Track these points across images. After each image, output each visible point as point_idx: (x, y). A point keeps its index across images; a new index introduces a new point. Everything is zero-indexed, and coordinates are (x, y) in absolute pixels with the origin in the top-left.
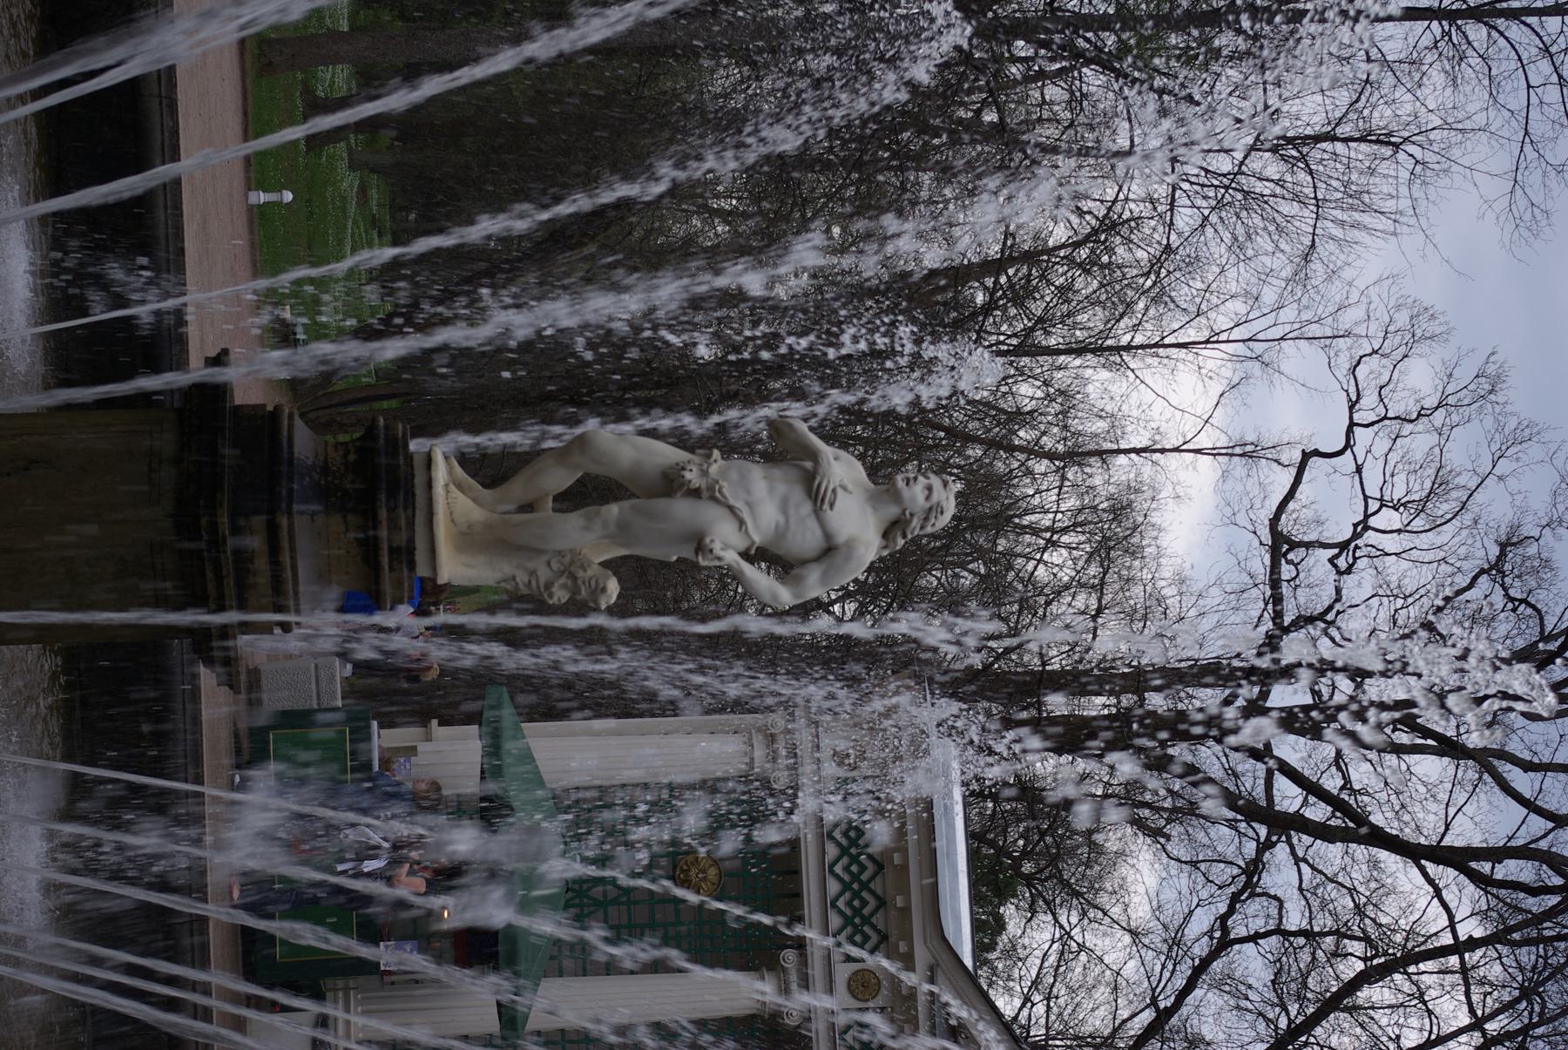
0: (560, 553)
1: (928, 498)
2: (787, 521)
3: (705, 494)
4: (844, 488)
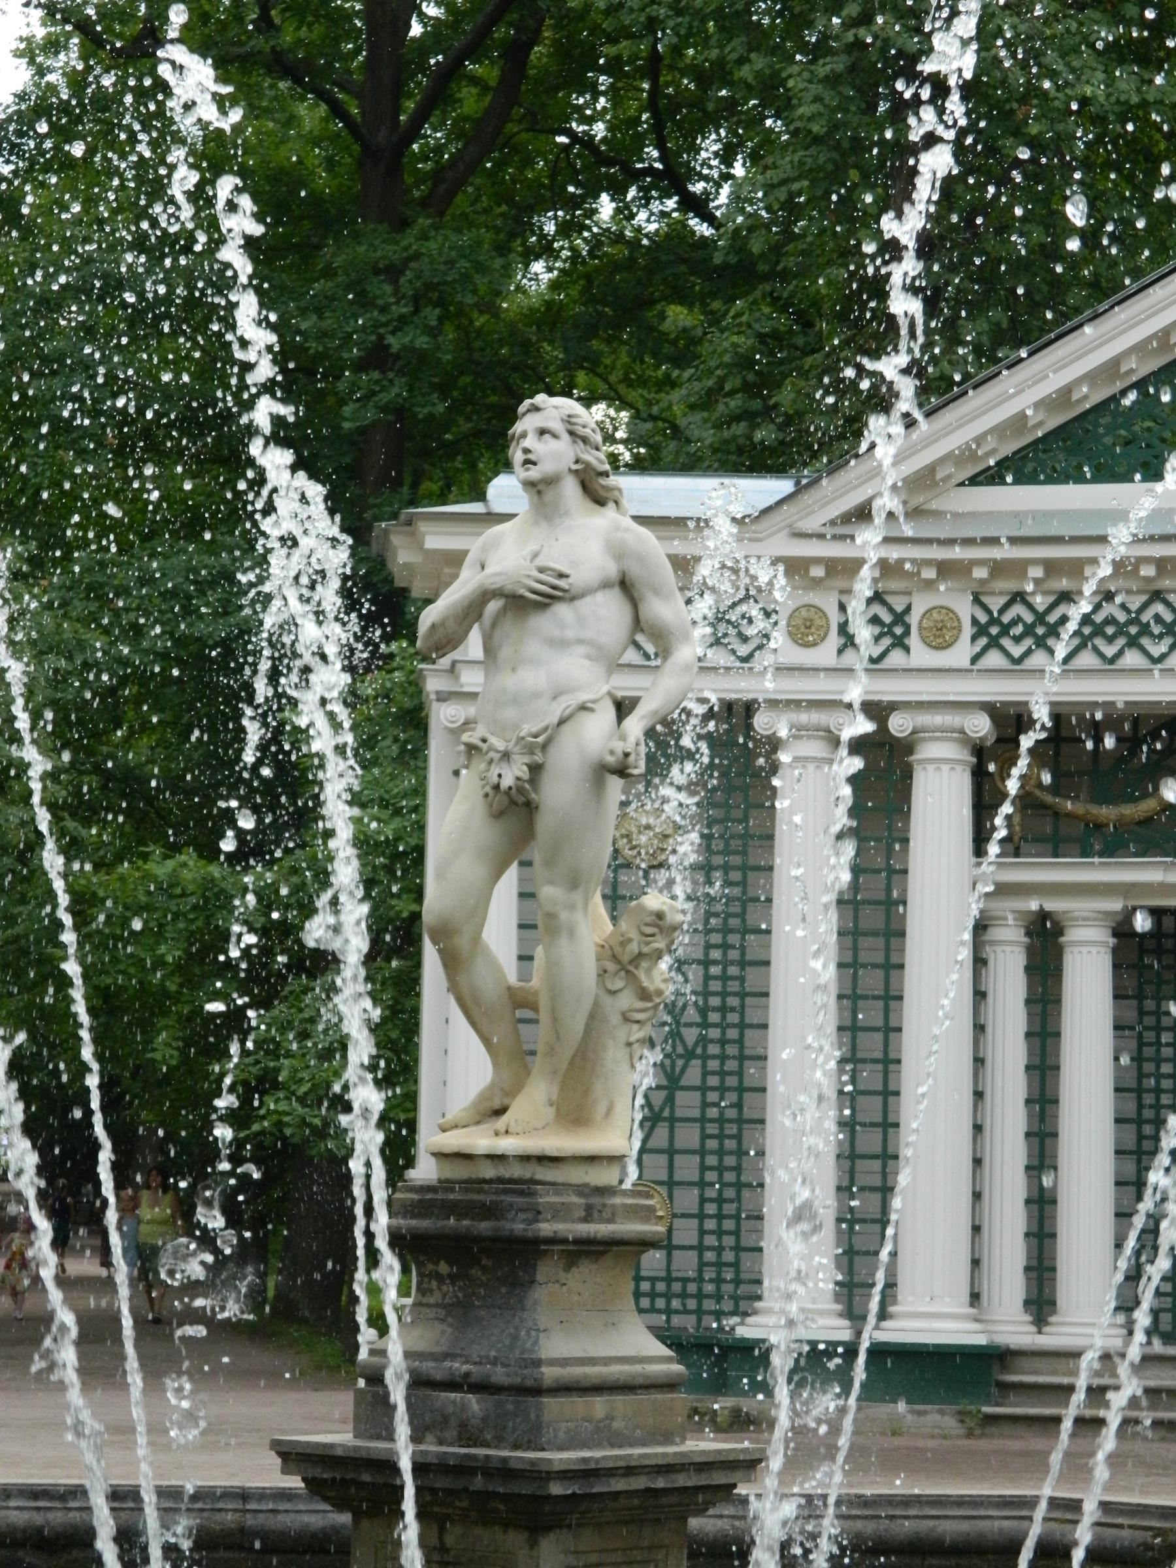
0: (603, 973)
1: (555, 436)
2: (580, 641)
3: (538, 758)
4: (535, 555)
